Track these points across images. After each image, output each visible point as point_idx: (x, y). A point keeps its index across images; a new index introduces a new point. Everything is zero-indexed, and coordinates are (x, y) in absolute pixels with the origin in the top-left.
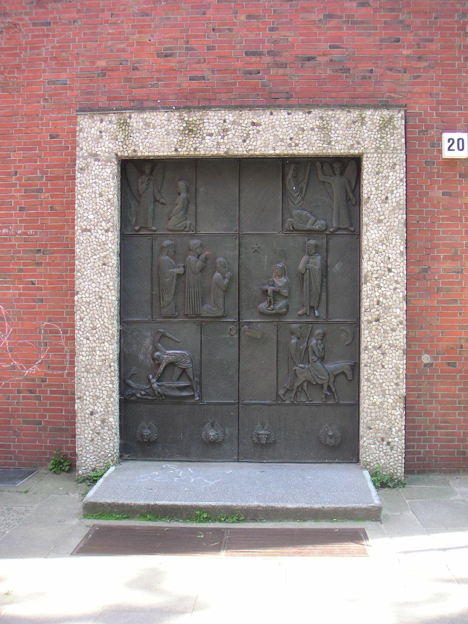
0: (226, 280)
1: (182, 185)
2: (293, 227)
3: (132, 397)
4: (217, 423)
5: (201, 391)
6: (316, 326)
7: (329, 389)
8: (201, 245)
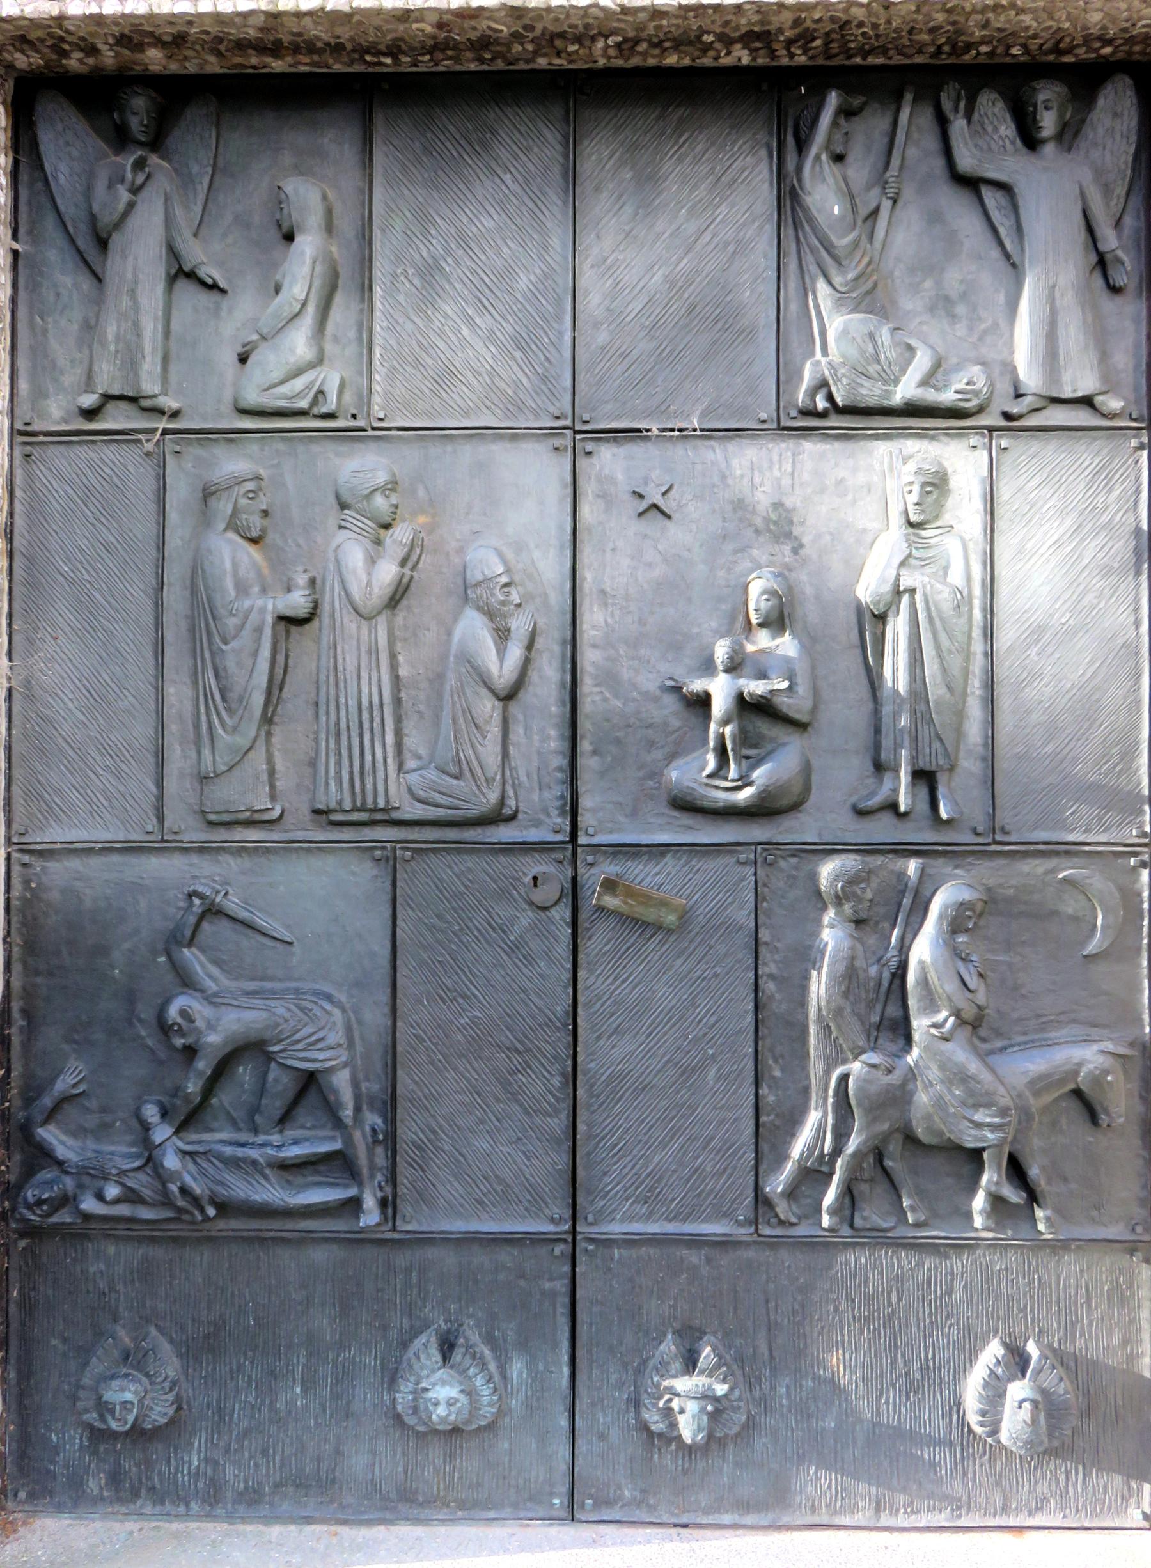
0: (515, 653)
1: (306, 196)
2: (830, 398)
3: (54, 1210)
4: (473, 1335)
5: (393, 1180)
6: (940, 866)
7: (1016, 1170)
8: (392, 486)
